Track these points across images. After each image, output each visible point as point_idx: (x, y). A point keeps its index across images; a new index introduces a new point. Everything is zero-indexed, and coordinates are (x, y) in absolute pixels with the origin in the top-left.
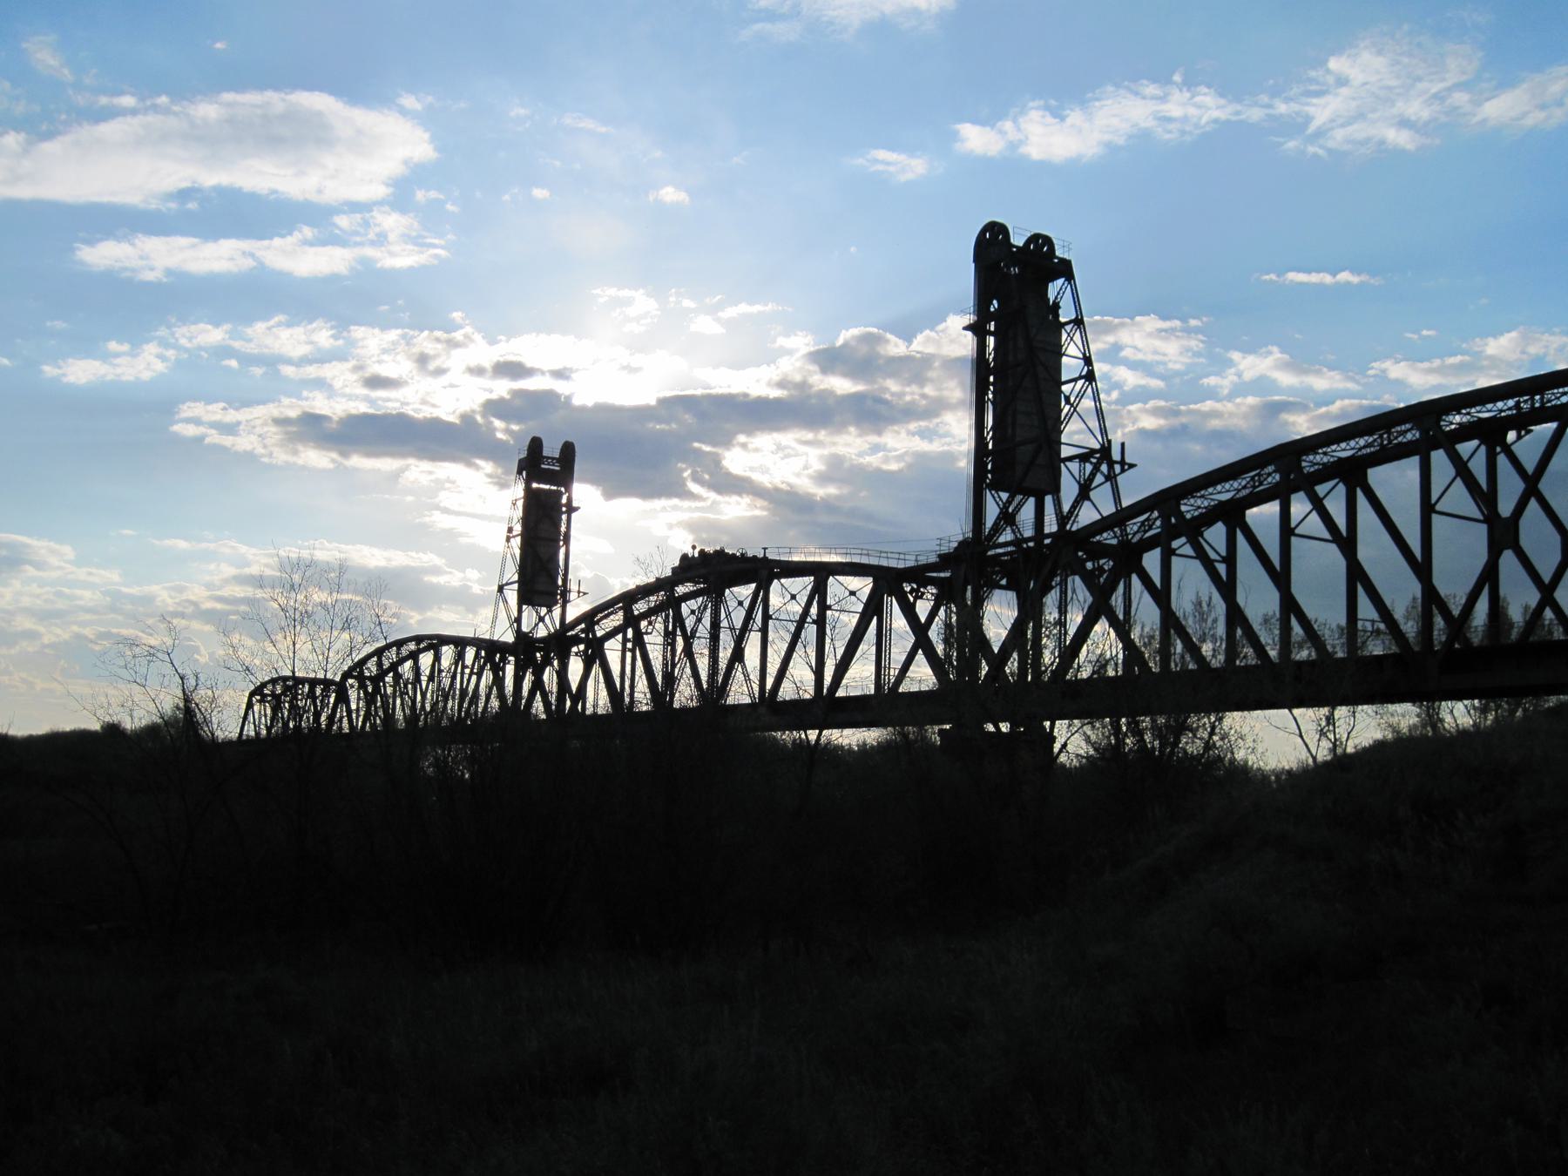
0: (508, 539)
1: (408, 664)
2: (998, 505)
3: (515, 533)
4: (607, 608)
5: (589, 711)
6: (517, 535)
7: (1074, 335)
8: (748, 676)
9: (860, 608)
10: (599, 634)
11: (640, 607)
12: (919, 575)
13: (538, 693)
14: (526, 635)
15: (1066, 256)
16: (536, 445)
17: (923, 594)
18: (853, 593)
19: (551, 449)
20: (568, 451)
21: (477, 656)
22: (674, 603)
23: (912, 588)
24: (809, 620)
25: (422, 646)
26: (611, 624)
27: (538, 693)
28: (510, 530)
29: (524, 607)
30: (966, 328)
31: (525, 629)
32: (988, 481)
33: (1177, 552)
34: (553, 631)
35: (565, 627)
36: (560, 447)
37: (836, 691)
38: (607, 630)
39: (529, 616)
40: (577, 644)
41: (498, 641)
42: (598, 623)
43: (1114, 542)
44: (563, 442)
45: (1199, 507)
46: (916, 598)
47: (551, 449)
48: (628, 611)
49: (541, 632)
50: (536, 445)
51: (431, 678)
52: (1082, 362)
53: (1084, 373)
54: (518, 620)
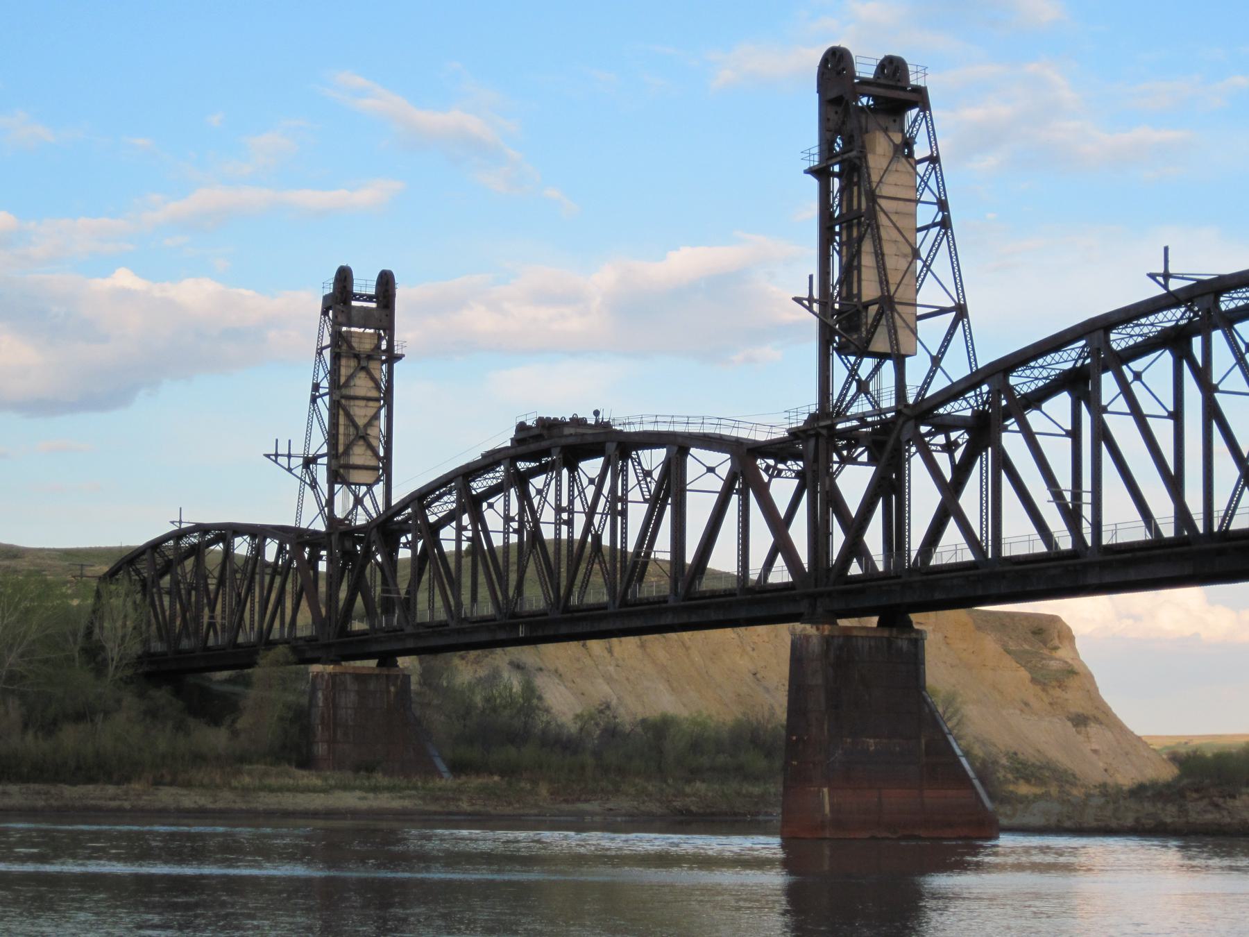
0: (314, 400)
1: (189, 563)
2: (847, 367)
3: (322, 391)
4: (438, 488)
5: (463, 616)
6: (325, 394)
7: (928, 179)
8: (586, 573)
11: (479, 486)
12: (779, 450)
13: (807, 570)
14: (341, 521)
15: (921, 83)
17: (780, 471)
18: (711, 470)
19: (365, 283)
20: (386, 282)
21: (281, 550)
22: (521, 481)
26: (485, 484)
27: (807, 570)
28: (316, 387)
29: (337, 487)
30: (806, 172)
31: (339, 513)
32: (835, 345)
34: (374, 515)
35: (391, 511)
38: (440, 515)
39: (345, 498)
40: (405, 533)
41: (307, 530)
42: (429, 505)
43: (968, 413)
44: (375, 277)
46: (771, 477)
47: (365, 283)
48: (465, 490)
49: (361, 520)
51: (221, 582)
52: (936, 208)
53: (939, 219)
54: (330, 502)
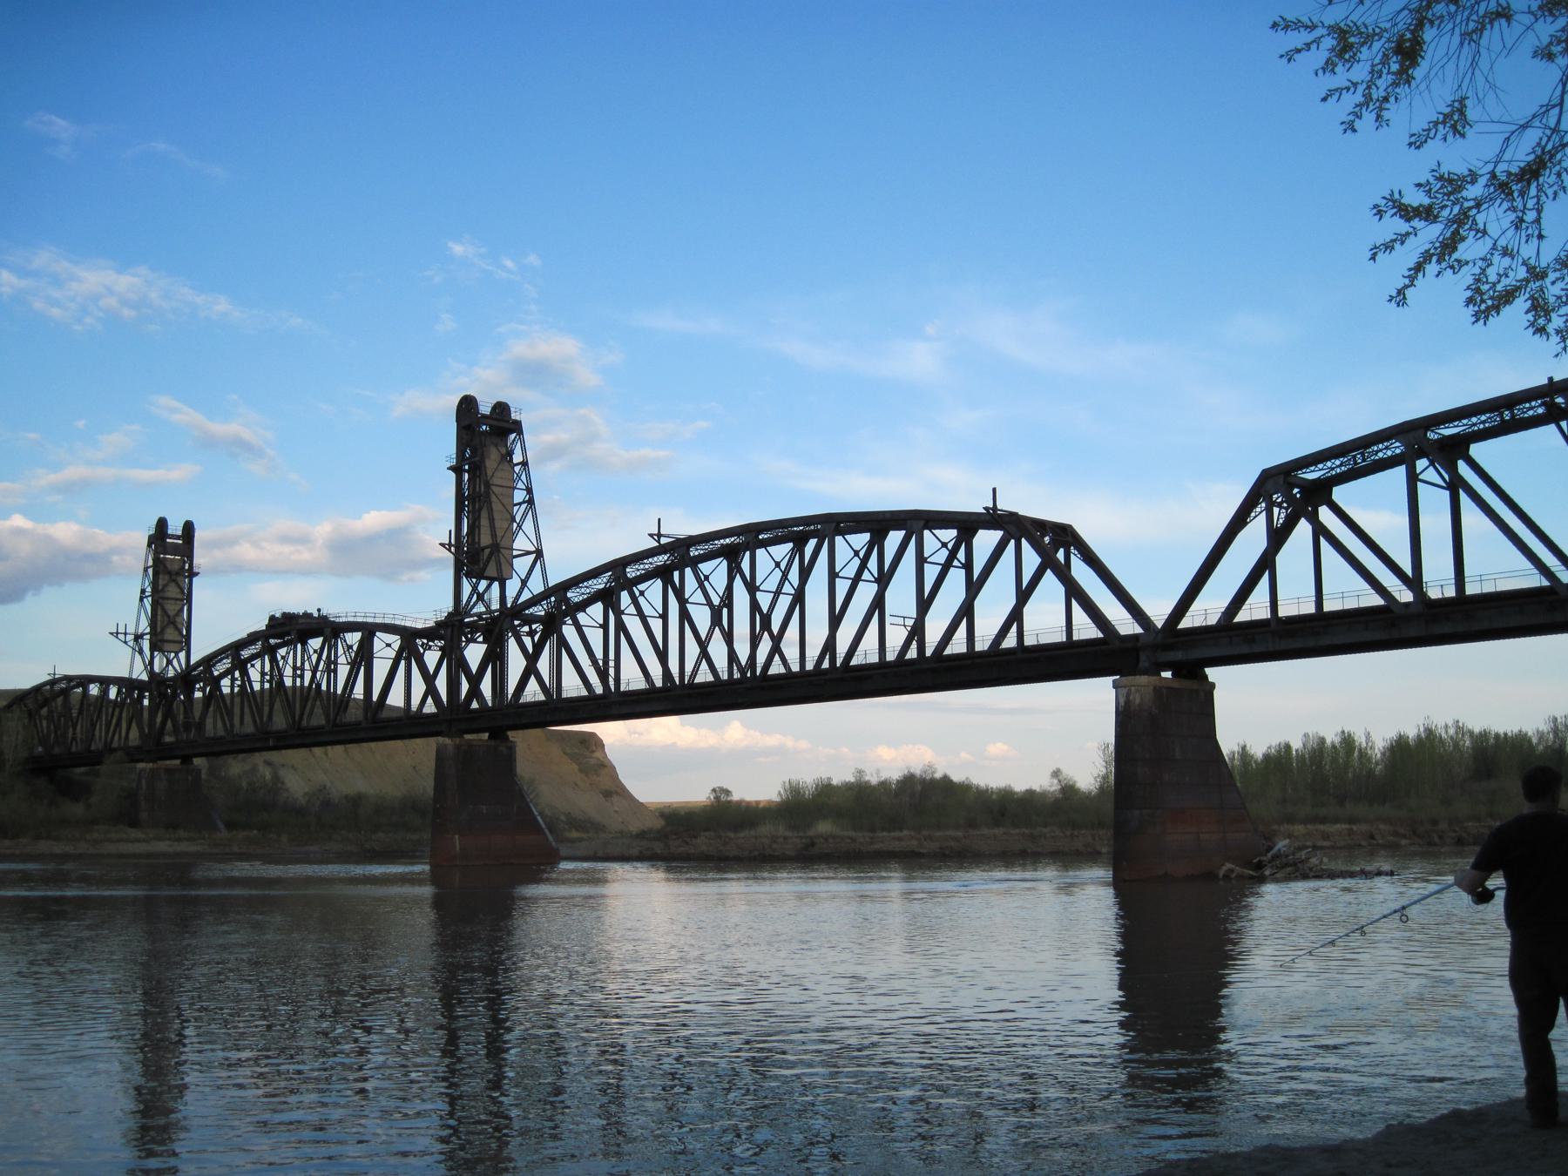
0: (141, 599)
3: (147, 594)
9: (393, 654)
10: (216, 673)
11: (245, 653)
15: (518, 418)
16: (162, 524)
18: (388, 645)
19: (175, 528)
22: (272, 651)
23: (423, 643)
24: (956, 563)
25: (72, 684)
28: (143, 591)
29: (156, 653)
33: (928, 560)
34: (179, 671)
36: (182, 525)
37: (1236, 614)
42: (214, 665)
43: (543, 613)
45: (583, 594)
47: (175, 528)
50: (162, 524)
53: (527, 499)
54: (151, 662)
